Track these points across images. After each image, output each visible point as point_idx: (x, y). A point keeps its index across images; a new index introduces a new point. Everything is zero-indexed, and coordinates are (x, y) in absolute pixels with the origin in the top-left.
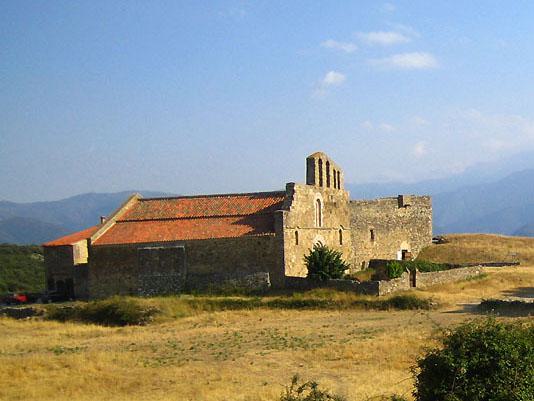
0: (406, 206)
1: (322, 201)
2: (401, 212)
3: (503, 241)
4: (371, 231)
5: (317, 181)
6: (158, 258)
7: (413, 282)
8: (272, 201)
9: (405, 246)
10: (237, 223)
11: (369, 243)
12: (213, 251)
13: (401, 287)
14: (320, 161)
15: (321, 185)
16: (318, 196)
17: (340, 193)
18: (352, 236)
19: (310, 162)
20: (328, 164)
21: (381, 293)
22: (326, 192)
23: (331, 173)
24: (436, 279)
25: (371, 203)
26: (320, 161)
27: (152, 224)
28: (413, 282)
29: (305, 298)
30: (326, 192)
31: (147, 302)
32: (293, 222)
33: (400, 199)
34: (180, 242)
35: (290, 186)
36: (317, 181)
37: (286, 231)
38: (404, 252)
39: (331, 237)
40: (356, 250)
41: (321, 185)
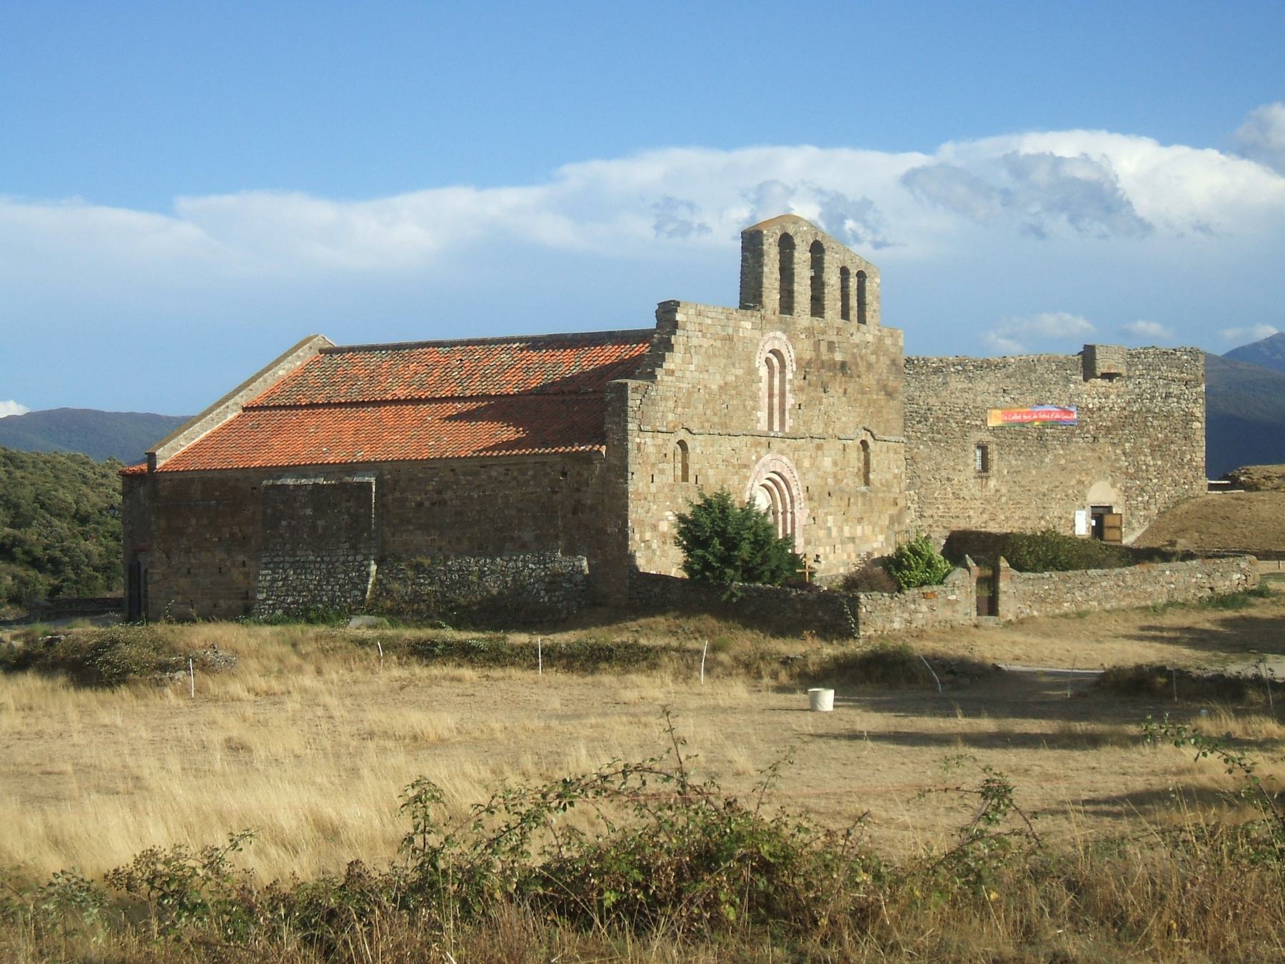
0: (1109, 376)
1: (790, 355)
2: (1091, 393)
3: (1027, 414)
4: (983, 448)
5: (772, 296)
6: (309, 512)
7: (990, 605)
8: (609, 354)
9: (1103, 492)
10: (460, 417)
11: (973, 487)
12: (448, 495)
13: (944, 613)
14: (786, 243)
15: (787, 305)
16: (777, 339)
17: (868, 334)
18: (911, 460)
19: (752, 241)
20: (817, 249)
21: (865, 631)
22: (810, 332)
23: (832, 278)
24: (1079, 595)
25: (986, 366)
26: (786, 243)
27: (325, 416)
28: (990, 605)
29: (617, 636)
30: (810, 332)
31: (201, 635)
32: (666, 413)
33: (1088, 355)
34: (366, 466)
35: (667, 312)
36: (772, 296)
37: (634, 439)
38: (1100, 514)
39: (827, 462)
40: (922, 501)
41: (787, 305)
